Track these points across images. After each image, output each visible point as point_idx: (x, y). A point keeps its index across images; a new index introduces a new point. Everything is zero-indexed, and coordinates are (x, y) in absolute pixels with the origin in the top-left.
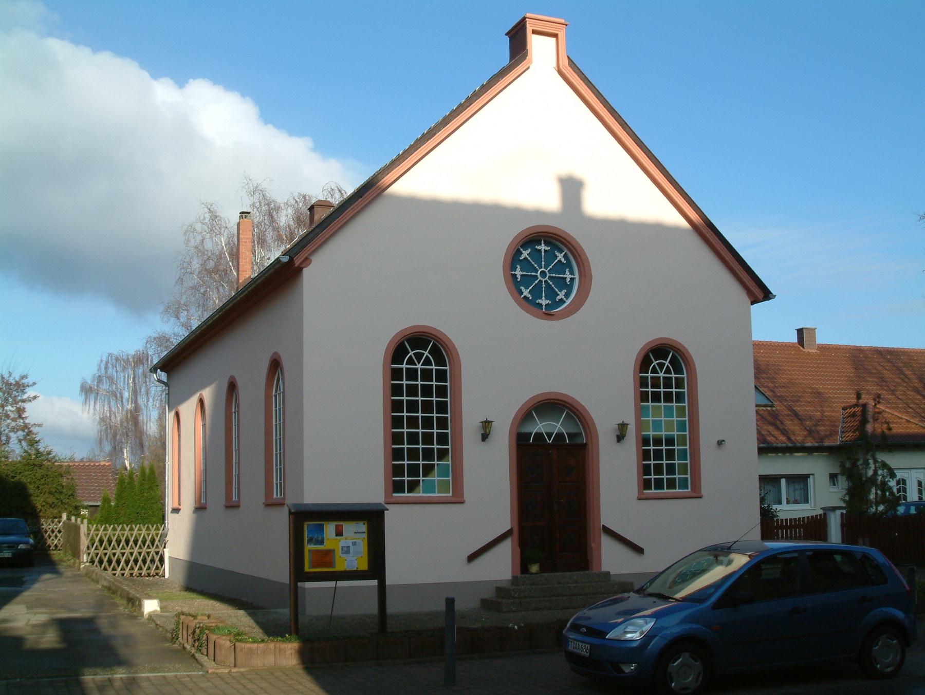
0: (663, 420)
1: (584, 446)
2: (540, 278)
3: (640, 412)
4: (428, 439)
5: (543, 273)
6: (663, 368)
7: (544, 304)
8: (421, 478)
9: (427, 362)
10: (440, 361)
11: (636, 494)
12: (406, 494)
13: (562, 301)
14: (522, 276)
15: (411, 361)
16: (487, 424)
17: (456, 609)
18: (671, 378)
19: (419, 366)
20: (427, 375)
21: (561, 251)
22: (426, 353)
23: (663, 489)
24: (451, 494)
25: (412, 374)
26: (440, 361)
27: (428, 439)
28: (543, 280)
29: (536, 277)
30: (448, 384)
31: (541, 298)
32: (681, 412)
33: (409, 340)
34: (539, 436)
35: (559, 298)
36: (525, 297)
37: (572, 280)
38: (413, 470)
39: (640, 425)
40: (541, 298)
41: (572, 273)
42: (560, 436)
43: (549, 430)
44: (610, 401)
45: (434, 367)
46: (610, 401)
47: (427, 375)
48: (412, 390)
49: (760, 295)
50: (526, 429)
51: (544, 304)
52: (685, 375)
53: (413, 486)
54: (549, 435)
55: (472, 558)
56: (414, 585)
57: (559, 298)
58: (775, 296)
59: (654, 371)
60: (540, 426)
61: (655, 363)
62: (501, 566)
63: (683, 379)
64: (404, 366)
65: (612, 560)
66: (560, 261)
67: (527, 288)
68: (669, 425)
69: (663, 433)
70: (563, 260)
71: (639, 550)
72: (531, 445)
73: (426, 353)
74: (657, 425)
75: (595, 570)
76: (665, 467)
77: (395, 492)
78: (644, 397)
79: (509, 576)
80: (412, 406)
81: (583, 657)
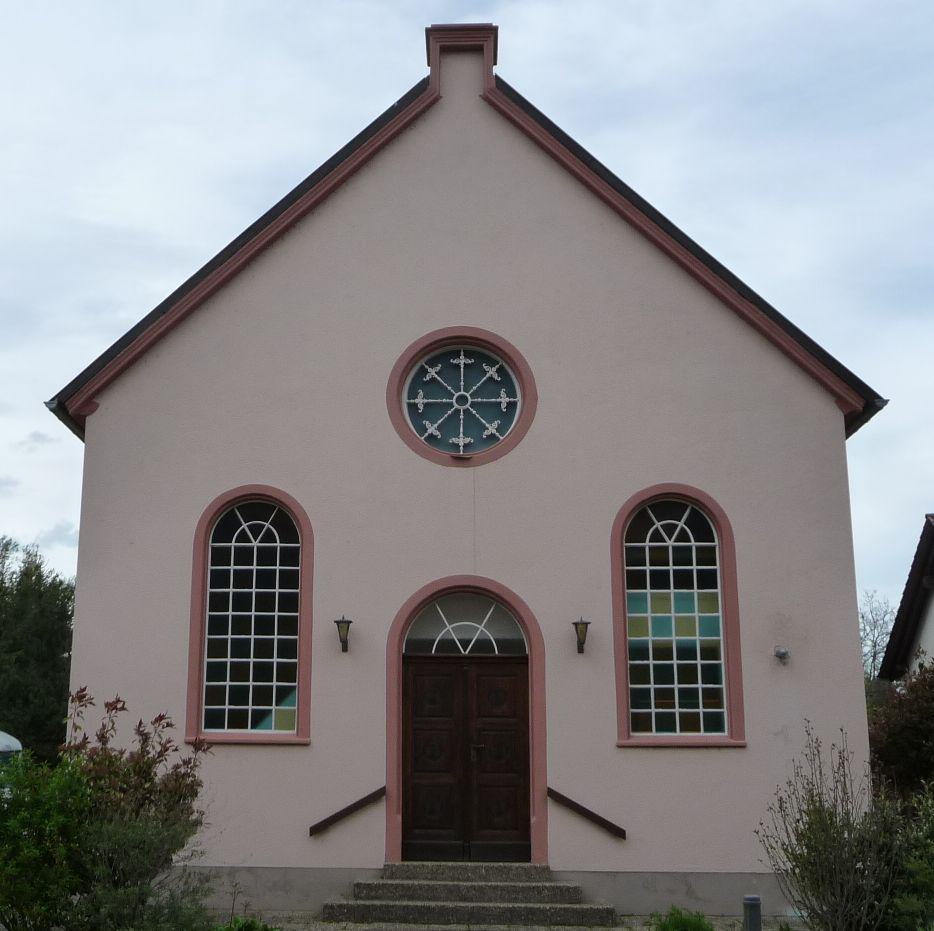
1: (524, 661)
3: (625, 605)
4: (264, 649)
6: (670, 538)
8: (273, 707)
9: (683, 537)
10: (703, 533)
12: (249, 731)
14: (426, 405)
15: (657, 537)
16: (581, 628)
18: (689, 549)
20: (266, 556)
21: (492, 363)
22: (245, 526)
24: (726, 733)
25: (244, 556)
26: (703, 533)
27: (264, 649)
29: (451, 405)
31: (457, 436)
32: (710, 603)
33: (653, 508)
34: (447, 645)
36: (431, 435)
38: (263, 696)
39: (624, 624)
40: (457, 436)
42: (483, 645)
43: (466, 637)
48: (243, 579)
50: (423, 635)
52: (716, 543)
53: (259, 719)
54: (465, 644)
55: (318, 830)
58: (886, 402)
61: (658, 525)
62: (370, 846)
64: (647, 544)
65: (564, 848)
67: (432, 423)
68: (686, 626)
69: (674, 639)
70: (496, 377)
71: (618, 833)
72: (433, 658)
73: (245, 526)
74: (686, 626)
75: (535, 863)
76: (677, 696)
77: (635, 729)
78: (636, 580)
79: (555, 862)
80: (242, 602)
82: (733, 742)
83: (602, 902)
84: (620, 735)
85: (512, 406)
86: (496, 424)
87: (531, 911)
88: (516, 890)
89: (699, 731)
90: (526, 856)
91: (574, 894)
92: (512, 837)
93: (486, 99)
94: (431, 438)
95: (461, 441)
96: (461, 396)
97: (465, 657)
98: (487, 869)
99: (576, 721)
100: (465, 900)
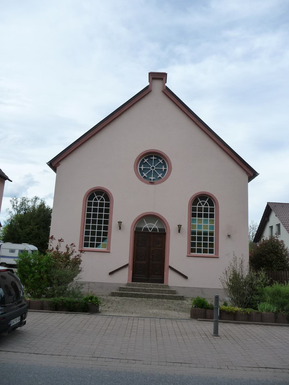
0: (203, 225)
1: (165, 234)
2: (153, 170)
3: (191, 222)
5: (153, 168)
6: (203, 205)
8: (101, 243)
9: (206, 205)
11: (186, 254)
16: (180, 226)
19: (99, 201)
20: (101, 205)
23: (195, 252)
24: (214, 254)
25: (96, 204)
28: (153, 170)
30: (214, 213)
34: (146, 229)
37: (165, 170)
39: (190, 226)
41: (165, 167)
42: (155, 229)
45: (209, 207)
47: (101, 205)
51: (152, 179)
53: (98, 245)
54: (150, 229)
55: (111, 273)
60: (147, 225)
63: (214, 208)
66: (160, 163)
68: (206, 227)
71: (186, 277)
74: (206, 227)
76: (202, 244)
78: (194, 215)
81: (219, 322)
85: (165, 170)
86: (161, 174)
87: (163, 296)
88: (160, 290)
89: (207, 253)
90: (162, 281)
91: (174, 292)
94: (145, 177)
95: (152, 178)
96: (153, 167)
98: (153, 285)
99: (177, 249)
100: (147, 292)
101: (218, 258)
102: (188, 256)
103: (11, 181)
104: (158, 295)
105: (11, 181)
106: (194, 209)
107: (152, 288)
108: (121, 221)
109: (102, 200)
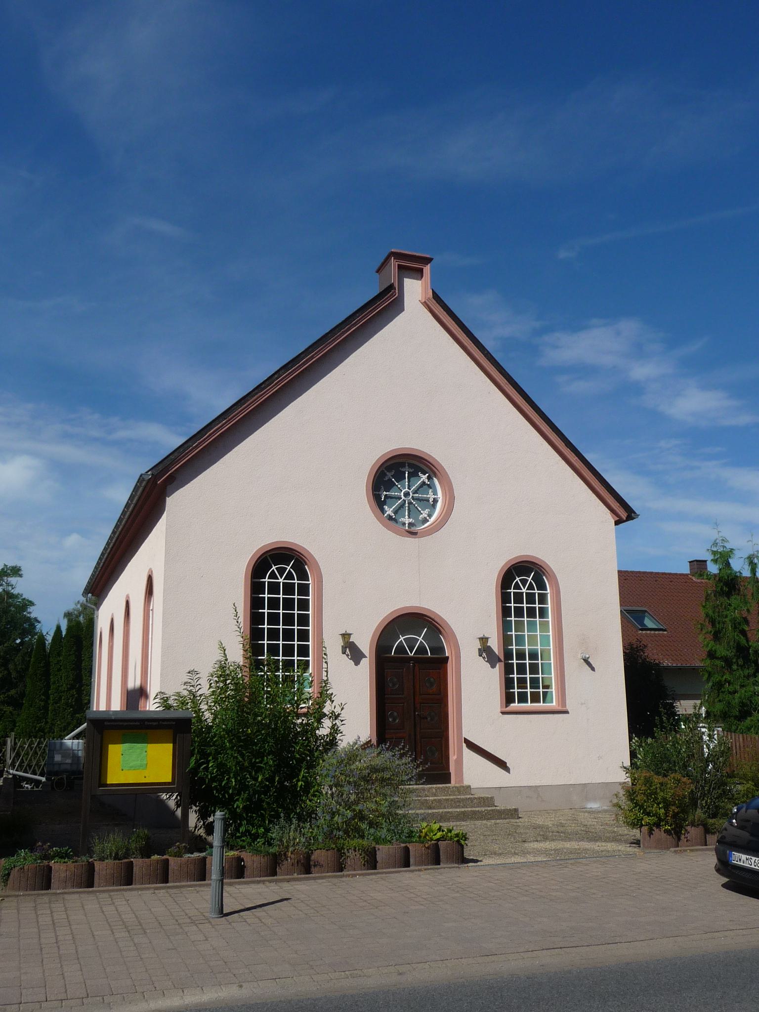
5: (407, 494)
7: (407, 522)
10: (303, 575)
13: (425, 521)
17: (170, 746)
23: (527, 702)
24: (554, 704)
31: (404, 517)
35: (431, 500)
40: (404, 517)
41: (435, 493)
44: (470, 618)
46: (470, 618)
49: (624, 515)
51: (407, 522)
56: (620, 590)
57: (431, 500)
59: (517, 587)
61: (518, 579)
65: (473, 773)
66: (424, 483)
71: (501, 764)
72: (393, 657)
76: (522, 682)
82: (560, 708)
83: (501, 805)
84: (501, 707)
85: (435, 501)
86: (427, 511)
87: (474, 812)
88: (459, 801)
89: (527, 702)
90: (446, 778)
91: (488, 801)
92: (437, 770)
93: (425, 304)
94: (390, 518)
95: (407, 520)
96: (403, 490)
97: (411, 658)
98: (436, 789)
99: (475, 695)
100: (430, 808)
101: (567, 712)
102: (503, 713)
103: (593, 669)
104: (464, 813)
105: (593, 669)
106: (505, 598)
107: (435, 795)
108: (348, 632)
109: (290, 576)
